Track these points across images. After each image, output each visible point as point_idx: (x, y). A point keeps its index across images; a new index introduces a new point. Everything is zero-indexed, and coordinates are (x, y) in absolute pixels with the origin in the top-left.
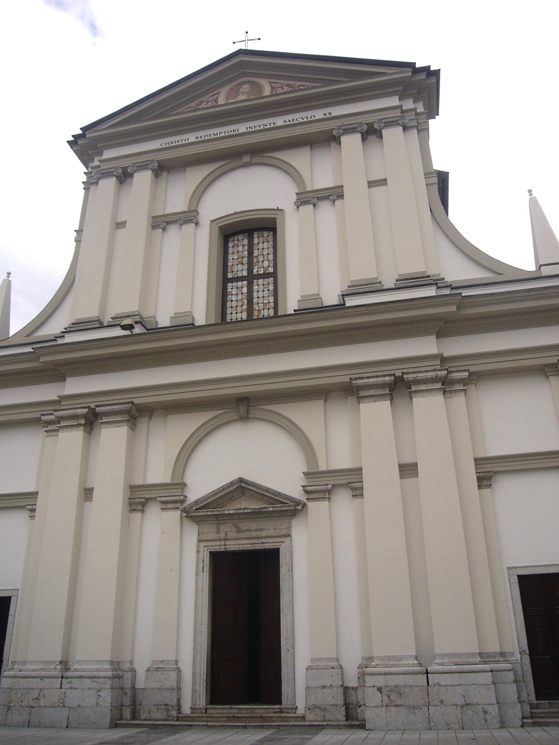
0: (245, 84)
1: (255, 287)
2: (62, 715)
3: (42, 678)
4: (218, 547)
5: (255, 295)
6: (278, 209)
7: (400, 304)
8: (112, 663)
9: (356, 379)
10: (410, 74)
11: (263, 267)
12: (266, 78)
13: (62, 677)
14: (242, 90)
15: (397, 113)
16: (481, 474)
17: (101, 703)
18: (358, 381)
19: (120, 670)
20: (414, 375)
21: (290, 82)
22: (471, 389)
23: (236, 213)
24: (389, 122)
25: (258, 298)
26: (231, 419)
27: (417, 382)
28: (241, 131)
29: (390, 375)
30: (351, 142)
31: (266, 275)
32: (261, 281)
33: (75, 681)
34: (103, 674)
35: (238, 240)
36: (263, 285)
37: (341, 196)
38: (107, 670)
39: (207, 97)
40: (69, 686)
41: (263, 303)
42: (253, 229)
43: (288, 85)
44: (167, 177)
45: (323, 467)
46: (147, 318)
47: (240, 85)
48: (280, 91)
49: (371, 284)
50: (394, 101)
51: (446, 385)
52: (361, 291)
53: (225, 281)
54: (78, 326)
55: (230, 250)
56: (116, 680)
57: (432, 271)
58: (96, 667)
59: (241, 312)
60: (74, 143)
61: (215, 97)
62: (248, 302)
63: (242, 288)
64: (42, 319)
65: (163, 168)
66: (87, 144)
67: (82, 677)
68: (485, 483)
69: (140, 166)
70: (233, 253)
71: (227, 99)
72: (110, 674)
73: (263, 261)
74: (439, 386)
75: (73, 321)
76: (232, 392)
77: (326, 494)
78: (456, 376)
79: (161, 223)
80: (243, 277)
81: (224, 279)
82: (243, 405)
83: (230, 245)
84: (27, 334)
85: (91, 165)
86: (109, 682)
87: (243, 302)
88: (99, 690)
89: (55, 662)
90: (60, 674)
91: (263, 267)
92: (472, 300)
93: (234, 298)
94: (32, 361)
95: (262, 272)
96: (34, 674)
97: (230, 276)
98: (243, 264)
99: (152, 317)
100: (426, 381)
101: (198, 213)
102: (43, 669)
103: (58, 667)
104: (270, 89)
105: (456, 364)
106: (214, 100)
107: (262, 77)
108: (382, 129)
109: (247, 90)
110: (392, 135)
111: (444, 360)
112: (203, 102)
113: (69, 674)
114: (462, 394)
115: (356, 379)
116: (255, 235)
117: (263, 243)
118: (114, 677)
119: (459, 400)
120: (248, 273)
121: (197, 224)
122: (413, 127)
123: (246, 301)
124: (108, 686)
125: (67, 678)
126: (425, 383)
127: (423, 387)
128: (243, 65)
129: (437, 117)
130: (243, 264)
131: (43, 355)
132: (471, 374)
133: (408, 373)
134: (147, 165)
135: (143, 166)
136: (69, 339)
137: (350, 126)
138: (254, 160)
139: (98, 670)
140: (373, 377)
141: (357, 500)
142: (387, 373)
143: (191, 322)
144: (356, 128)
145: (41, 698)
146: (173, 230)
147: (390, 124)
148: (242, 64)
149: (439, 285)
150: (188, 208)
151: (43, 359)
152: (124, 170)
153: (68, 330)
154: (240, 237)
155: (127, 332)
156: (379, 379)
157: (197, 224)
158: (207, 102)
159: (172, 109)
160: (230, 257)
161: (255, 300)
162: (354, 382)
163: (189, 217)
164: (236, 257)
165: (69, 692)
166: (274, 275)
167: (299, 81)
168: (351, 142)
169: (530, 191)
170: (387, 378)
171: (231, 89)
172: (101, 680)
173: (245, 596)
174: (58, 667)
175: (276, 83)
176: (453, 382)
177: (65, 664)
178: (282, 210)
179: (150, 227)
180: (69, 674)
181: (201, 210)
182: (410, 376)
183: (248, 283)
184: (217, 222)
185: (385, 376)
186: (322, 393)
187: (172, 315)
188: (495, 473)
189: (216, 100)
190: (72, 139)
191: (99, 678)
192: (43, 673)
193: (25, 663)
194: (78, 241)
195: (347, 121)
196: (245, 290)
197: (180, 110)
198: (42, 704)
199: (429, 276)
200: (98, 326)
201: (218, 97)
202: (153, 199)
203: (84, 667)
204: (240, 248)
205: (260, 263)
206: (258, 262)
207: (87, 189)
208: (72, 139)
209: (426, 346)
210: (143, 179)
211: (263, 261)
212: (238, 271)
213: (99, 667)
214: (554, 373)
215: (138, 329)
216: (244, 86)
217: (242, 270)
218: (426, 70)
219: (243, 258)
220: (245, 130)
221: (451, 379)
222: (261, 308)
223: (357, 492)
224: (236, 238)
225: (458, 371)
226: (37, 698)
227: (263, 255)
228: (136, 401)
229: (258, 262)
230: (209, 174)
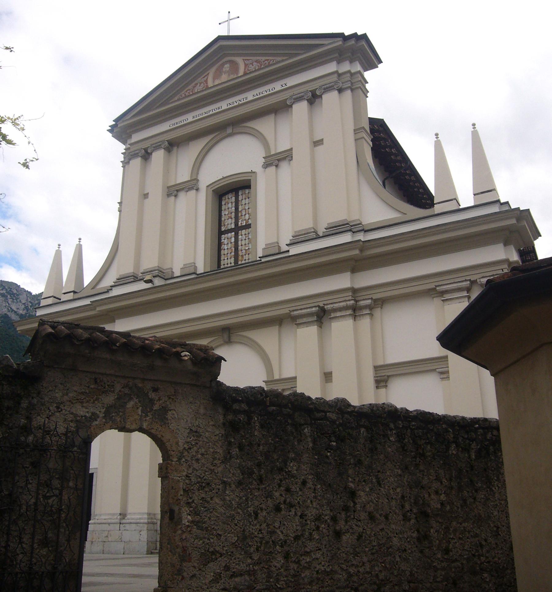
0: (226, 64)
1: (240, 237)
2: (120, 546)
3: (109, 524)
5: (240, 243)
6: (252, 172)
7: (313, 253)
8: (149, 514)
9: (294, 311)
10: (341, 43)
11: (245, 220)
12: (241, 56)
13: (120, 523)
14: (224, 70)
15: (334, 78)
16: (378, 378)
17: (142, 539)
18: (295, 313)
19: (155, 519)
20: (332, 306)
21: (258, 58)
22: (377, 312)
23: (224, 178)
24: (327, 88)
25: (242, 245)
26: (219, 343)
27: (335, 310)
28: (223, 108)
29: (315, 307)
30: (301, 108)
32: (244, 232)
33: (126, 525)
34: (142, 521)
35: (228, 198)
36: (245, 234)
38: (145, 519)
39: (200, 79)
40: (124, 528)
41: (245, 250)
42: (236, 189)
43: (256, 61)
44: (177, 151)
45: (276, 377)
46: (167, 269)
47: (223, 65)
48: (252, 68)
49: (307, 233)
50: (331, 67)
51: (355, 311)
52: (300, 240)
53: (221, 233)
54: (122, 281)
55: (223, 207)
56: (152, 525)
57: (354, 217)
58: (139, 517)
59: (231, 258)
60: (112, 129)
61: (205, 79)
62: (235, 250)
63: (231, 238)
64: (102, 274)
65: (172, 145)
66: (122, 128)
67: (131, 523)
68: (383, 384)
69: (156, 147)
70: (225, 210)
71: (214, 79)
72: (146, 521)
73: (245, 215)
74: (350, 312)
75: (118, 277)
76: (218, 325)
78: (362, 303)
79: (173, 191)
80: (231, 229)
81: (218, 232)
83: (223, 203)
84: (93, 286)
85: (129, 142)
86: (146, 526)
87: (232, 250)
88: (140, 531)
89: (117, 514)
90: (118, 521)
91: (245, 220)
92: (372, 243)
93: (226, 248)
94: (92, 310)
95: (244, 224)
96: (104, 521)
97: (223, 229)
98: (232, 218)
99: (169, 269)
100: (340, 309)
101: (198, 180)
102: (110, 519)
103: (119, 517)
104: (244, 65)
105: (364, 293)
106: (205, 81)
107: (237, 56)
108: (322, 95)
109: (228, 69)
110: (330, 99)
111: (354, 291)
112: (197, 84)
113: (124, 521)
114: (368, 317)
115: (294, 311)
116: (240, 193)
117: (245, 199)
118: (148, 523)
119: (365, 322)
120: (235, 225)
121: (197, 190)
122: (346, 89)
123: (233, 249)
124: (145, 528)
125: (123, 524)
126: (340, 311)
127: (338, 314)
128: (223, 49)
129: (380, 66)
130: (232, 218)
131: (98, 306)
132: (375, 301)
133: (327, 304)
134: (160, 145)
135: (158, 146)
136: (116, 292)
137: (299, 95)
138: (236, 130)
139: (140, 519)
140: (304, 309)
141: (445, 382)
142: (313, 305)
143: (193, 271)
144: (303, 96)
145: (109, 536)
146: (182, 195)
147: (328, 89)
148: (221, 48)
149: (354, 230)
150: (191, 177)
151: (98, 309)
152: (146, 150)
153: (117, 284)
154: (230, 196)
155: (149, 285)
156: (309, 310)
157: (197, 190)
158: (200, 83)
159: (172, 97)
160: (223, 214)
161: (240, 248)
162: (292, 313)
163: (191, 185)
164: (227, 213)
165: (124, 532)
167: (265, 56)
168: (301, 108)
169: (437, 135)
170: (314, 309)
171: (217, 69)
172: (141, 525)
174: (119, 517)
175: (248, 60)
176: (362, 308)
177: (123, 515)
178: (254, 172)
179: (166, 196)
180: (124, 521)
181: (200, 177)
182: (329, 306)
183: (235, 234)
184: (211, 186)
185: (312, 307)
186: (278, 321)
187: (182, 266)
188: (393, 376)
189: (206, 81)
190: (110, 128)
191: (140, 523)
192: (109, 521)
193: (101, 515)
194: (120, 211)
195: (296, 91)
196: (233, 240)
197: (176, 98)
198: (110, 540)
199: (348, 224)
200: (132, 280)
201: (207, 79)
202: (167, 172)
203: (133, 517)
204: (230, 205)
205: (243, 217)
206: (242, 215)
207: (123, 167)
208: (110, 128)
209: (342, 281)
210: (158, 156)
211: (245, 215)
212: (228, 224)
213: (140, 517)
214: (436, 295)
215: (158, 282)
216: (226, 66)
217: (231, 224)
218: (354, 36)
219: (231, 213)
220: (226, 107)
221: (359, 306)
222: (244, 254)
223: (445, 376)
224: (227, 196)
225: (364, 300)
226: (107, 537)
227: (245, 209)
228: (158, 335)
229: (242, 215)
230: (202, 150)
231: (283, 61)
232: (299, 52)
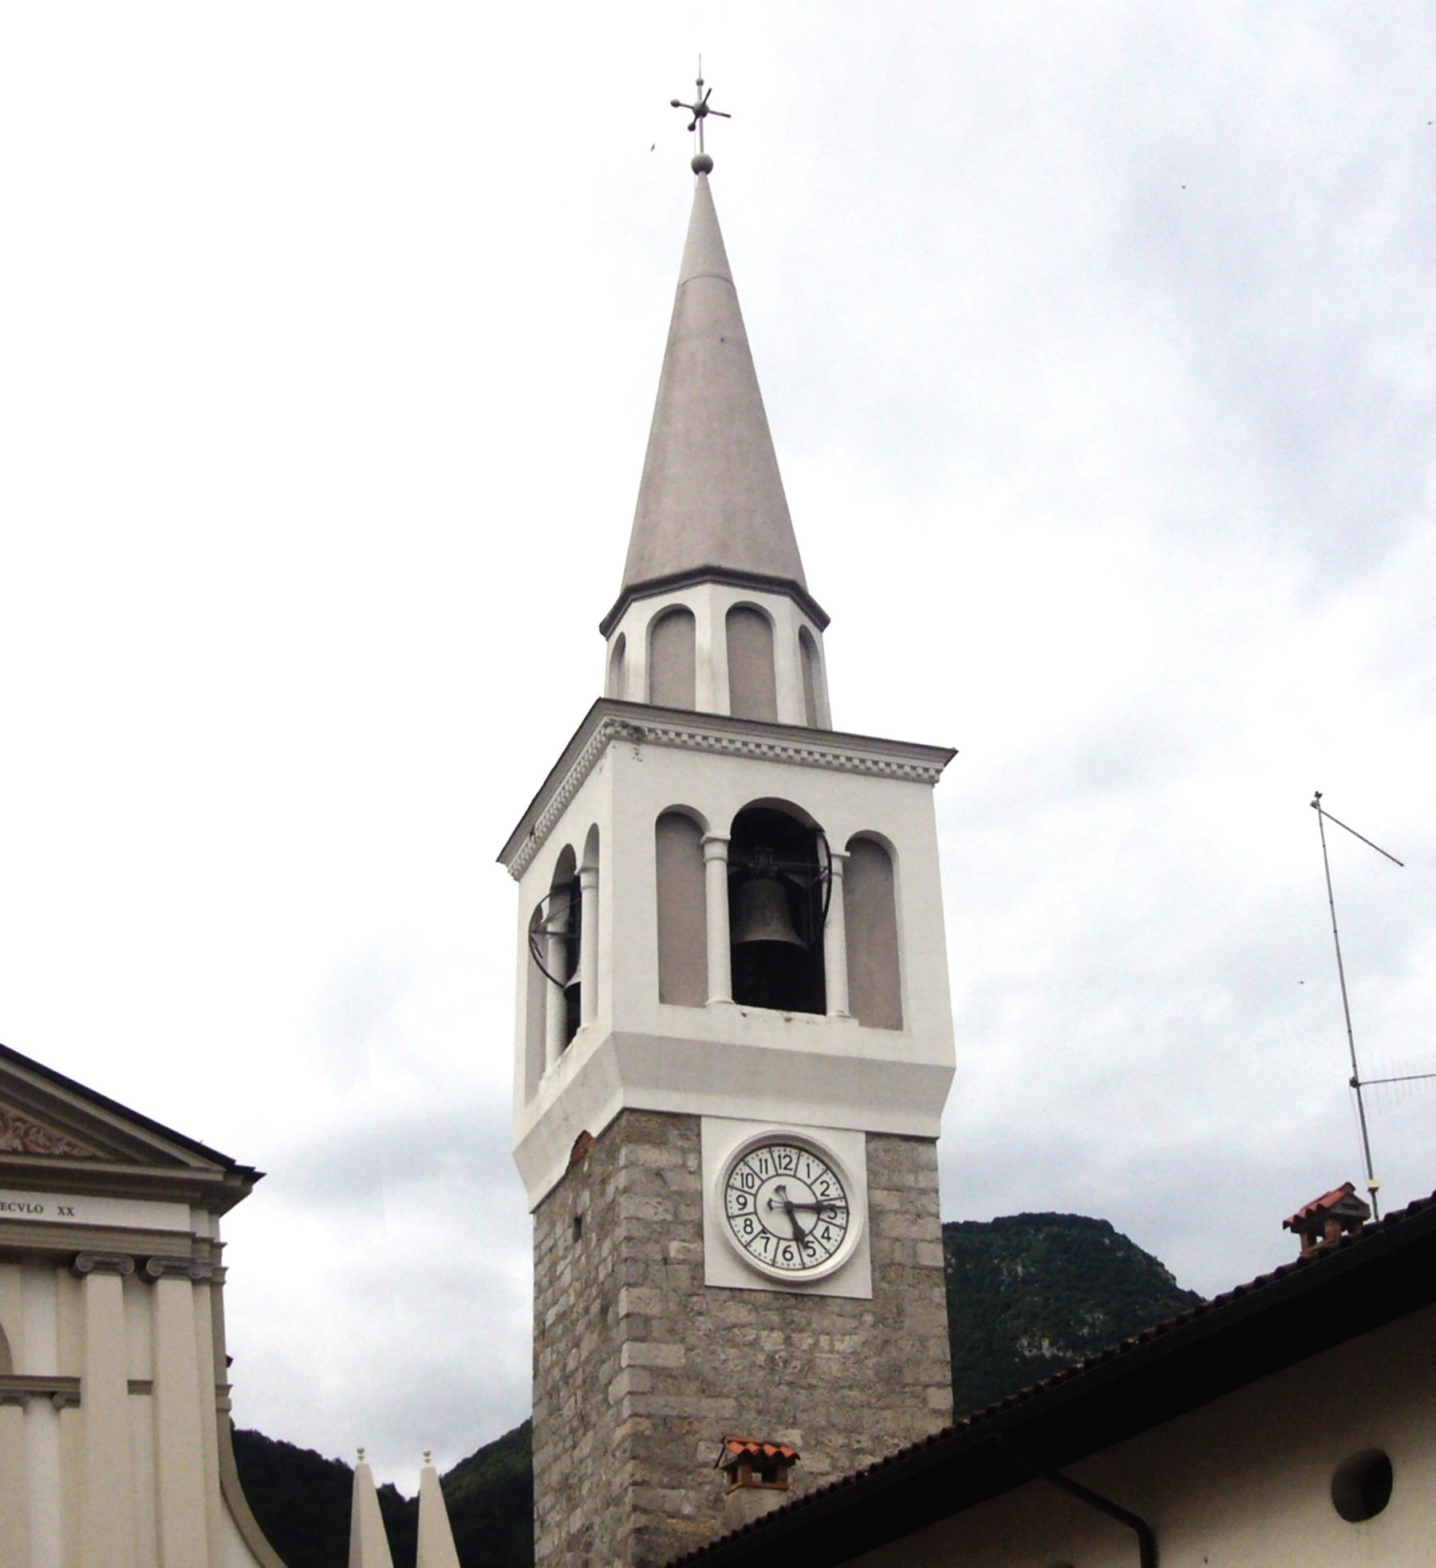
24: (174, 1267)
37: (74, 1401)
231: (93, 1158)
232: (138, 1157)
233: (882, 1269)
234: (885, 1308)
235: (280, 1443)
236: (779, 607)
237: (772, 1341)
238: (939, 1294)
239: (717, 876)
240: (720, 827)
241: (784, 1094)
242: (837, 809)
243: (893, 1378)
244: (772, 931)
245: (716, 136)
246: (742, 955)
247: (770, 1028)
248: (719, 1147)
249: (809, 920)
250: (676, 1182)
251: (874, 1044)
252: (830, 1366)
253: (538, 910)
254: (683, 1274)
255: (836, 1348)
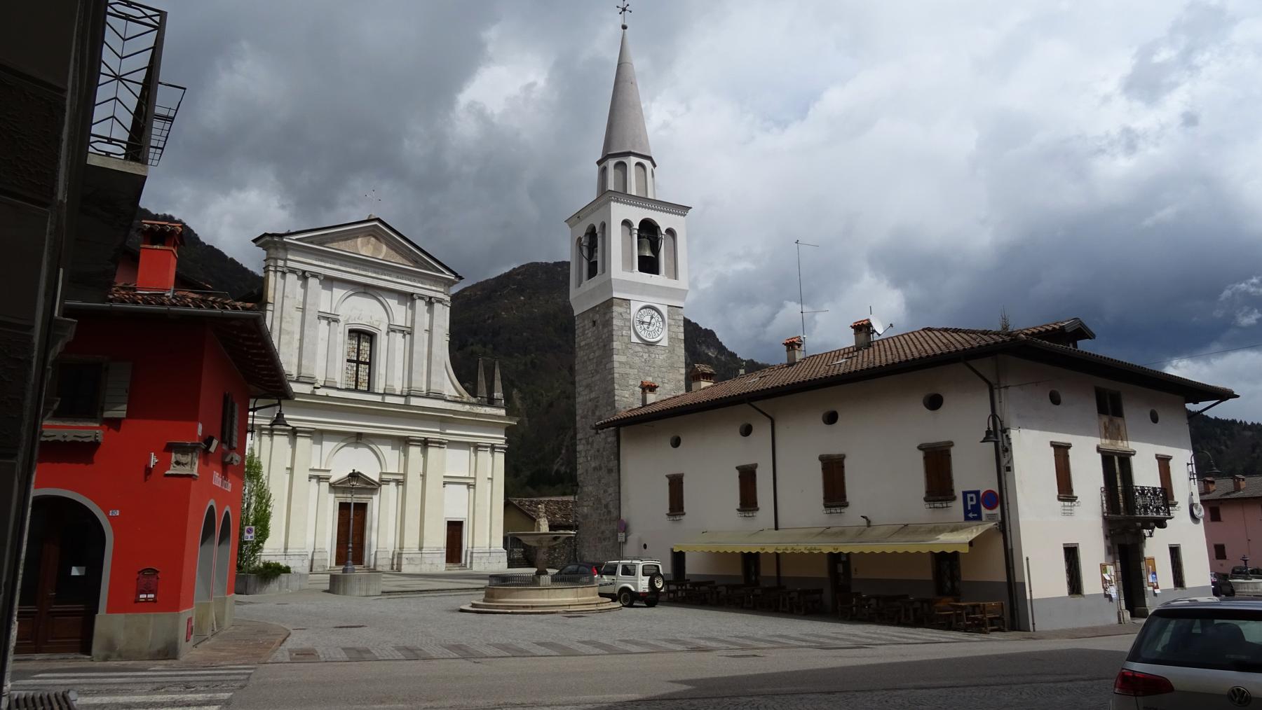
4: (343, 500)
31: (365, 363)
77: (388, 482)
82: (358, 439)
166: (369, 364)
168: (415, 451)
173: (352, 524)
233: (670, 339)
234: (671, 349)
235: (232, 260)
236: (647, 163)
237: (646, 356)
238: (683, 345)
239: (636, 237)
240: (636, 226)
241: (649, 295)
242: (664, 221)
243: (672, 366)
244: (648, 253)
245: (629, 19)
246: (641, 258)
247: (647, 278)
248: (635, 307)
249: (655, 248)
250: (625, 316)
251: (671, 283)
252: (658, 362)
253: (580, 239)
254: (626, 339)
255: (661, 357)
